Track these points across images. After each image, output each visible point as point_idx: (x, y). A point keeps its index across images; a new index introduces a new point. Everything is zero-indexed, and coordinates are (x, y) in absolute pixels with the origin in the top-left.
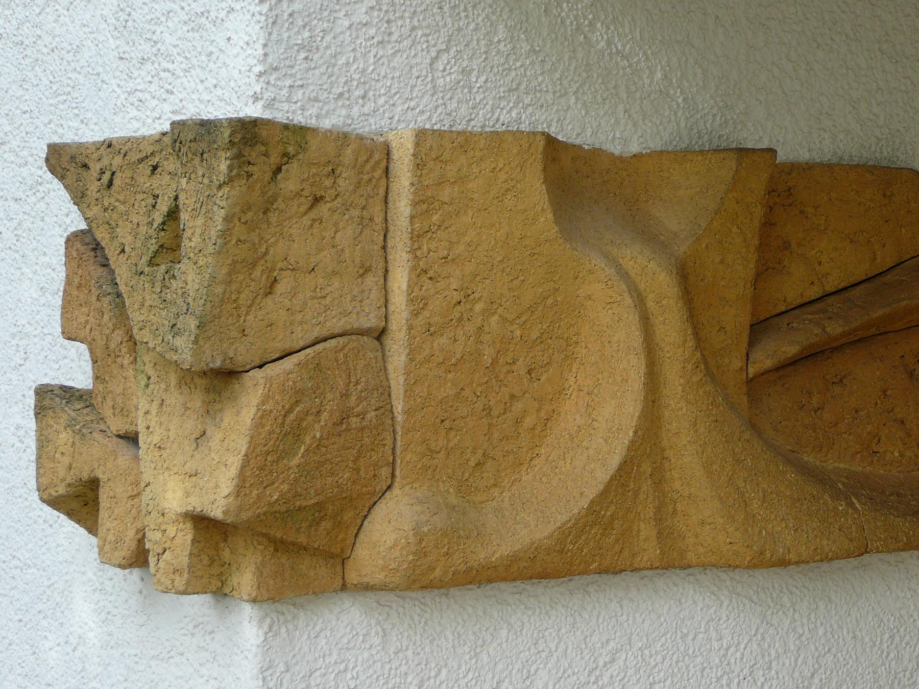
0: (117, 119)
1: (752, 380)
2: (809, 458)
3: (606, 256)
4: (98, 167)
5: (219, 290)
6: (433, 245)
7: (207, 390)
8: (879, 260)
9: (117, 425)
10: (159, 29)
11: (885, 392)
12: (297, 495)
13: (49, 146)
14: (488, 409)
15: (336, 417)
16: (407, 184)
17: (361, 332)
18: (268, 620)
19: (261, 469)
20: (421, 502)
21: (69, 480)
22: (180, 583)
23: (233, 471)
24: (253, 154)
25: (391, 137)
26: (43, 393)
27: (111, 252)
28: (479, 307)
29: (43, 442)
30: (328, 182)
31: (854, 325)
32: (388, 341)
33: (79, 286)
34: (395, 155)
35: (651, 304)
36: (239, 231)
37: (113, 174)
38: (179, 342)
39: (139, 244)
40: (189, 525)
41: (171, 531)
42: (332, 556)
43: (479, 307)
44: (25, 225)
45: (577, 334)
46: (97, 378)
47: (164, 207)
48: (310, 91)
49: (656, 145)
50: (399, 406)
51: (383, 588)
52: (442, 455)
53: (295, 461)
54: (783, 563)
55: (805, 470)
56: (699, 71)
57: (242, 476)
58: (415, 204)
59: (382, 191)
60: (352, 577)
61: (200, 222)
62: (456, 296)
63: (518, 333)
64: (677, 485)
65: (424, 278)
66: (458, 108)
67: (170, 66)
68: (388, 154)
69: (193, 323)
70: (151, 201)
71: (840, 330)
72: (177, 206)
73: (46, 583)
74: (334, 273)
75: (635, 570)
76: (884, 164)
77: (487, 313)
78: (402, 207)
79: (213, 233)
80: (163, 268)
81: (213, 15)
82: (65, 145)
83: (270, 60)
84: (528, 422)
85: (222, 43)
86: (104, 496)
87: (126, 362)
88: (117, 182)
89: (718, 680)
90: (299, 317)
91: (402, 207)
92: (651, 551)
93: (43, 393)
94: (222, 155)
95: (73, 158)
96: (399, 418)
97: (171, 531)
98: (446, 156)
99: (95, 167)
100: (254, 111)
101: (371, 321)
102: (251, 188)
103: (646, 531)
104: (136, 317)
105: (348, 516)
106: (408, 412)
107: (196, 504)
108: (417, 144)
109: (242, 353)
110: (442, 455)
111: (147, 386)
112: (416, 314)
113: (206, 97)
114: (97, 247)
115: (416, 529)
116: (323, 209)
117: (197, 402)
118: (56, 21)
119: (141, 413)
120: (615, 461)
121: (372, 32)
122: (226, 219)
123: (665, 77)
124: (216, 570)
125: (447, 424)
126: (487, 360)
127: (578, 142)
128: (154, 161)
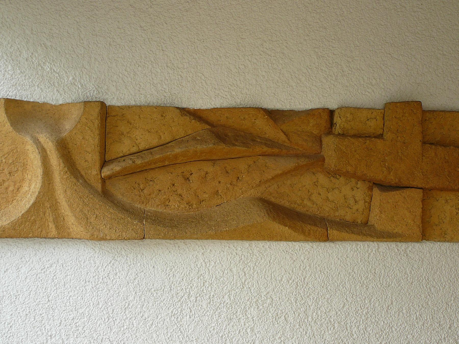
84: (11, 188)
92: (53, 232)
120: (31, 202)
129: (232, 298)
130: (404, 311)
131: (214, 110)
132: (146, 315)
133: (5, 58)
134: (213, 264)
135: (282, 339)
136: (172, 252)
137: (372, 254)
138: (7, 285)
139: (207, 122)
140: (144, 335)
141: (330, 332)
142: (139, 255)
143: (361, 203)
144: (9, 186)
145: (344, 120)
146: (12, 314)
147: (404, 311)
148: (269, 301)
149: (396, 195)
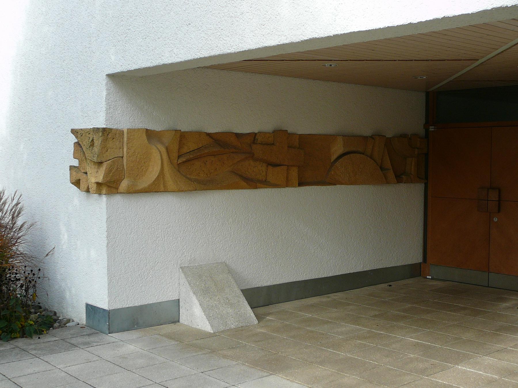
0: (81, 125)
1: (179, 164)
2: (188, 176)
3: (155, 146)
4: (80, 133)
5: (100, 151)
6: (130, 145)
7: (98, 165)
8: (199, 146)
9: (83, 171)
10: (89, 112)
11: (201, 166)
12: (111, 179)
13: (71, 129)
14: (138, 168)
15: (116, 169)
16: (126, 136)
17: (120, 157)
18: (107, 197)
19: (106, 175)
20: (128, 181)
21: (75, 180)
22: (94, 192)
23: (102, 176)
24: (104, 133)
25: (124, 129)
26: (71, 167)
27: (82, 146)
28: (136, 153)
29: (71, 174)
30: (115, 136)
31: (195, 156)
32: (123, 158)
33: (76, 151)
34: (124, 132)
35: (162, 153)
36: (103, 143)
37: (82, 134)
38: (94, 158)
39: (87, 144)
40: (96, 184)
41: (93, 185)
42: (116, 188)
43: (136, 153)
44: (64, 140)
45: (151, 157)
46: (79, 164)
47: (91, 139)
48: (112, 123)
49: (163, 129)
50: (125, 167)
51: (124, 193)
52: (131, 174)
53: (111, 175)
54: (183, 191)
55: (187, 178)
56: (170, 118)
57: (104, 177)
58: (127, 139)
59: (122, 137)
60: (119, 191)
61: (97, 142)
62: (133, 152)
63: (142, 157)
64: (166, 179)
65: (129, 149)
66: (133, 125)
67: (90, 118)
68: (123, 132)
69: (97, 156)
70: (89, 138)
71: (192, 157)
72: (93, 139)
73: (69, 197)
74: (116, 149)
75: (161, 192)
76: (200, 131)
77: (138, 154)
78: (125, 139)
79: (99, 143)
80: (91, 148)
81: (98, 111)
82: (74, 129)
83: (106, 119)
84: (144, 170)
85: (99, 116)
86: (81, 182)
87: (85, 162)
88: (83, 135)
89: (174, 209)
90: (111, 155)
91: (125, 139)
92: (162, 189)
93: (71, 167)
94: (101, 133)
95: (75, 131)
96: (125, 169)
97: (93, 185)
98: (131, 132)
99: (79, 133)
100: (104, 126)
101: (121, 155)
102: (104, 137)
103: (162, 186)
104: (87, 155)
105: (118, 183)
106: (126, 168)
107: (97, 181)
108: (127, 131)
109: (103, 160)
110: (131, 174)
111: (88, 165)
112: (127, 154)
113: (96, 123)
114: (79, 144)
115: (128, 184)
116: (114, 140)
117: (96, 167)
118: (70, 108)
119: (87, 169)
120: (157, 176)
121: (121, 114)
122: (101, 141)
123: (165, 119)
124: (99, 191)
125: (132, 170)
126: (138, 161)
127: (151, 129)
128: (89, 132)
129: (223, 215)
130: (280, 217)
131: (216, 133)
132: (193, 225)
133: (138, 109)
134: (216, 200)
135: (241, 231)
136: (202, 196)
137: (269, 193)
138: (140, 215)
139: (212, 138)
140: (193, 233)
141: (256, 227)
142: (190, 198)
143: (264, 172)
144: (143, 169)
145: (262, 137)
146: (142, 228)
147: (280, 217)
148: (236, 215)
149: (278, 169)
